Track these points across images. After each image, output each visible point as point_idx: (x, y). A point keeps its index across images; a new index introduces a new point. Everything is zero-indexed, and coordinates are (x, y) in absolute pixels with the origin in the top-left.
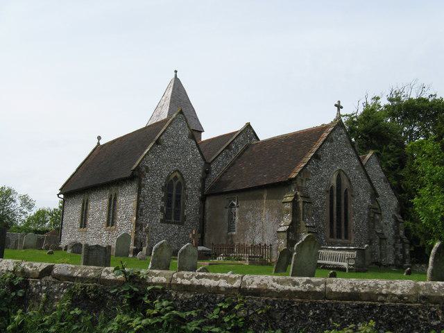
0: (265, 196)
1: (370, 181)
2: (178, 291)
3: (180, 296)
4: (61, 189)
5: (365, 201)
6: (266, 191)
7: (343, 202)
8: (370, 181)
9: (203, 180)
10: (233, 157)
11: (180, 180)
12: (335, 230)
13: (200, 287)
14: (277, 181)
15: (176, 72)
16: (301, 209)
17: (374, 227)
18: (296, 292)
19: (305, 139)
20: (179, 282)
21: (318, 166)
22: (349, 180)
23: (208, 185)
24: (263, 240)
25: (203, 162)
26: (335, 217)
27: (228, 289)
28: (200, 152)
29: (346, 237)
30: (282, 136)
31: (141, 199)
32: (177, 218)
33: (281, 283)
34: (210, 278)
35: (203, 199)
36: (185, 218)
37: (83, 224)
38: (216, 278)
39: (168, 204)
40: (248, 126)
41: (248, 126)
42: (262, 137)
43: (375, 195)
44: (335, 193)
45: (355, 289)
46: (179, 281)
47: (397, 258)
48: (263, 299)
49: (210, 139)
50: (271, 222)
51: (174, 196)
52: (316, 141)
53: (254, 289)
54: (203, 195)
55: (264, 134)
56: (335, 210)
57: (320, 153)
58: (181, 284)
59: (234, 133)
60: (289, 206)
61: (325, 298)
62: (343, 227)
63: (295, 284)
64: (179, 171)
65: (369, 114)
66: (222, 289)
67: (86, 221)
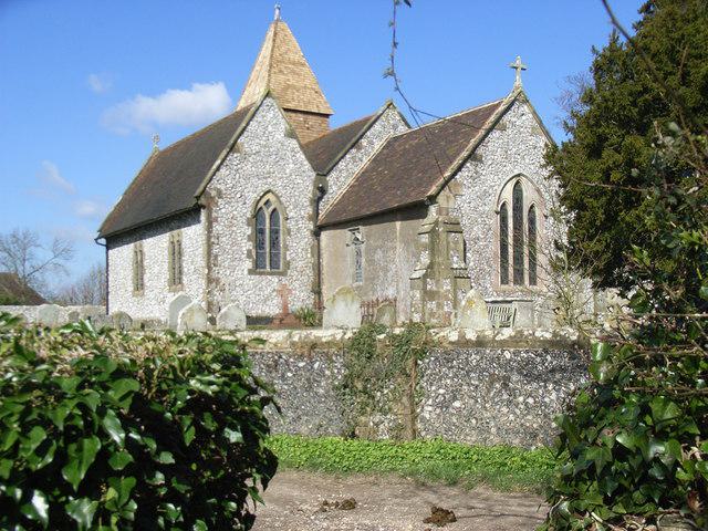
4: (100, 231)
9: (316, 202)
23: (324, 208)
35: (316, 234)
36: (288, 264)
37: (139, 286)
39: (259, 245)
44: (510, 212)
54: (316, 226)
56: (510, 240)
60: (425, 239)
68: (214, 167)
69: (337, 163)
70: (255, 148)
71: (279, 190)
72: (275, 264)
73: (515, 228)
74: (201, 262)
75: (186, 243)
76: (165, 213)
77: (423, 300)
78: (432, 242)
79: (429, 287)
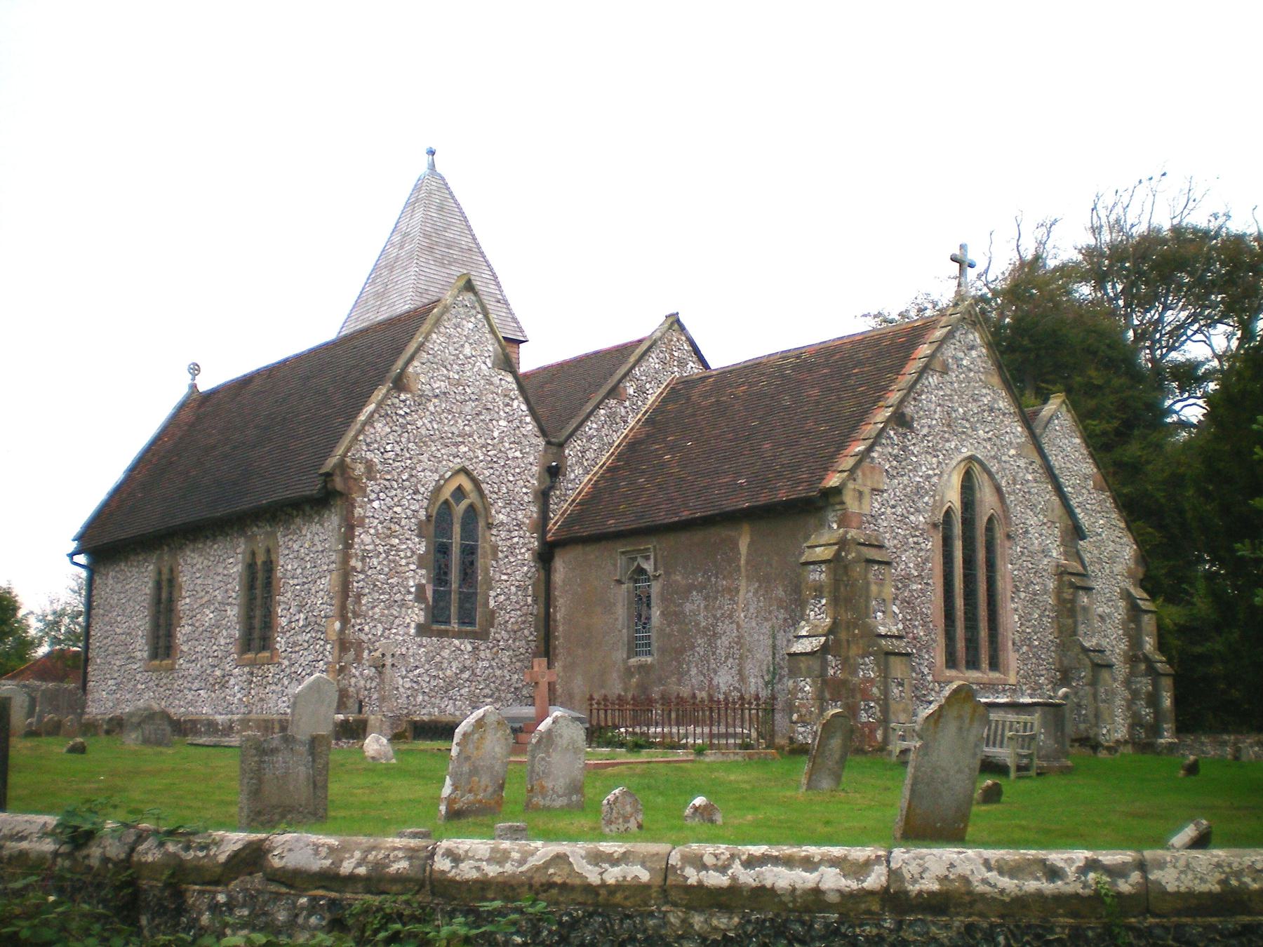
0: (744, 544)
1: (1059, 489)
2: (690, 908)
3: (698, 920)
4: (80, 538)
5: (1045, 552)
7: (981, 555)
8: (1059, 489)
9: (543, 497)
10: (632, 423)
11: (473, 497)
12: (960, 645)
13: (762, 893)
14: (782, 496)
17: (1075, 633)
18: (1059, 899)
19: (859, 363)
20: (692, 881)
21: (904, 449)
22: (998, 489)
23: (560, 508)
24: (742, 678)
25: (541, 442)
26: (959, 602)
27: (849, 897)
29: (994, 665)
30: (785, 355)
31: (353, 562)
32: (467, 617)
33: (1013, 871)
34: (789, 862)
35: (545, 556)
37: (163, 644)
38: (808, 864)
39: (440, 577)
40: (675, 323)
41: (675, 323)
43: (1076, 532)
45: (1234, 882)
46: (692, 876)
47: (1136, 723)
48: (958, 922)
51: (456, 551)
53: (932, 894)
55: (723, 353)
57: (909, 410)
58: (700, 886)
60: (819, 576)
61: (1148, 911)
62: (983, 633)
63: (1053, 873)
64: (464, 470)
66: (833, 898)
67: (170, 635)
68: (362, 417)
70: (440, 385)
71: (482, 472)
72: (467, 617)
75: (286, 565)
76: (246, 504)
77: (820, 698)
78: (836, 582)
79: (831, 672)
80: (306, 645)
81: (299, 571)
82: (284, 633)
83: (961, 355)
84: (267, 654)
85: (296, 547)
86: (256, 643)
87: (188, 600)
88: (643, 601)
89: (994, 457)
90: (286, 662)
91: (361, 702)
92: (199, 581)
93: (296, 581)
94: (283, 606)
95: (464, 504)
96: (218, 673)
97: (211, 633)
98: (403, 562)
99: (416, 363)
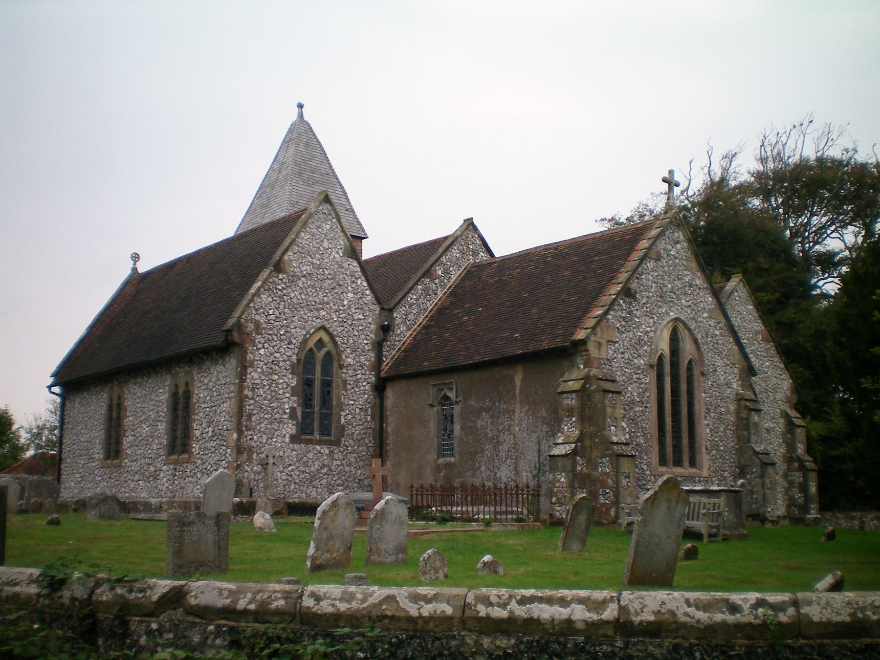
0: (518, 381)
1: (738, 341)
2: (481, 633)
3: (486, 641)
5: (728, 385)
6: (520, 368)
7: (684, 387)
8: (738, 341)
9: (378, 346)
10: (440, 295)
11: (330, 347)
12: (669, 449)
13: (531, 623)
14: (545, 345)
15: (301, 106)
16: (252, 291)
17: (749, 441)
18: (738, 626)
20: (482, 614)
21: (630, 313)
22: (695, 341)
23: (390, 355)
24: (517, 473)
25: (377, 308)
26: (668, 420)
27: (592, 625)
28: (370, 285)
29: (693, 463)
30: (547, 247)
31: (246, 392)
32: (325, 430)
33: (706, 607)
34: (549, 601)
35: (380, 388)
37: (113, 449)
38: (563, 602)
39: (307, 402)
40: (470, 224)
41: (470, 224)
42: (497, 254)
43: (750, 371)
45: (860, 615)
48: (668, 642)
49: (384, 255)
50: (535, 435)
52: (626, 257)
53: (649, 623)
55: (505, 242)
57: (633, 286)
58: (488, 617)
59: (446, 238)
60: (571, 401)
61: (800, 635)
62: (685, 441)
63: (734, 608)
64: (323, 328)
65: (717, 193)
66: (580, 626)
67: (118, 443)
69: (405, 295)
70: (306, 269)
71: (336, 329)
72: (325, 430)
73: (672, 391)
74: (224, 419)
75: (199, 394)
78: (583, 406)
79: (579, 468)
80: (213, 449)
81: (208, 398)
82: (198, 441)
83: (669, 247)
84: (186, 456)
85: (206, 381)
86: (179, 448)
87: (131, 418)
88: (448, 419)
89: (693, 319)
90: (199, 462)
91: (251, 489)
92: (139, 405)
93: (206, 405)
94: (197, 422)
95: (323, 351)
96: (152, 469)
97: (147, 441)
98: (281, 392)
99: (290, 253)
